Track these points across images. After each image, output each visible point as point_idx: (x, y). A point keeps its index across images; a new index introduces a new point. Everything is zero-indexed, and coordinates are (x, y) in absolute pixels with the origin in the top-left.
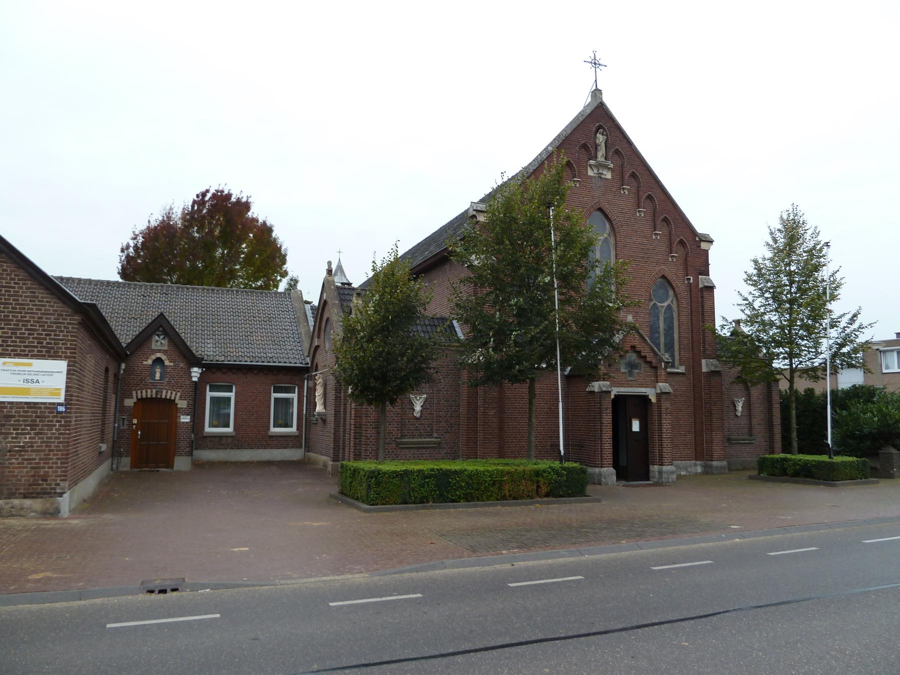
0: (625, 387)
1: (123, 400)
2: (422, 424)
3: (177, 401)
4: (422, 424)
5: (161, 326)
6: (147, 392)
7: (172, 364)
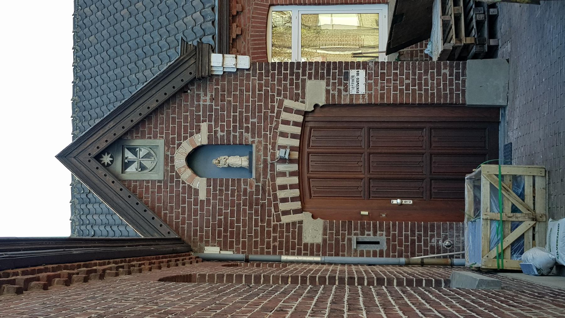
1: (306, 245)
3: (308, 107)
5: (98, 157)
6: (283, 187)
7: (204, 126)
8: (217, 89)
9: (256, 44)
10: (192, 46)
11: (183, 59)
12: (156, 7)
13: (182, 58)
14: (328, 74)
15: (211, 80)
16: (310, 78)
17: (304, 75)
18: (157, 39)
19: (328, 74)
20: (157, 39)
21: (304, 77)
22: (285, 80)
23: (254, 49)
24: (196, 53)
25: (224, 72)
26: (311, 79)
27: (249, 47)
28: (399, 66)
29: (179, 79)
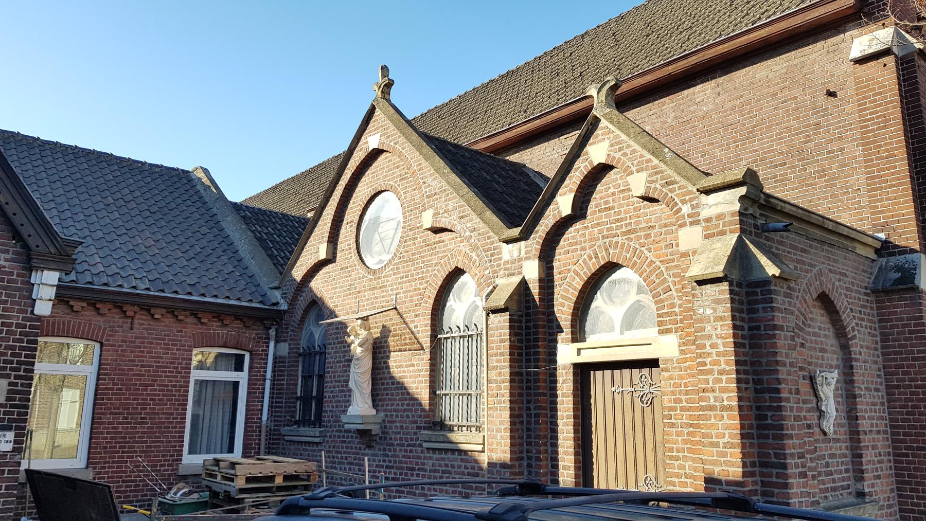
8: (12, 274)
9: (59, 324)
10: (73, 252)
11: (56, 239)
12: (113, 229)
13: (59, 239)
14: (12, 406)
15: (24, 269)
16: (10, 384)
17: (16, 377)
18: (78, 226)
19: (12, 406)
20: (78, 226)
21: (12, 377)
22: (12, 355)
23: (54, 323)
24: (62, 255)
25: (33, 285)
26: (9, 386)
27: (56, 317)
28: (10, 492)
29: (32, 232)
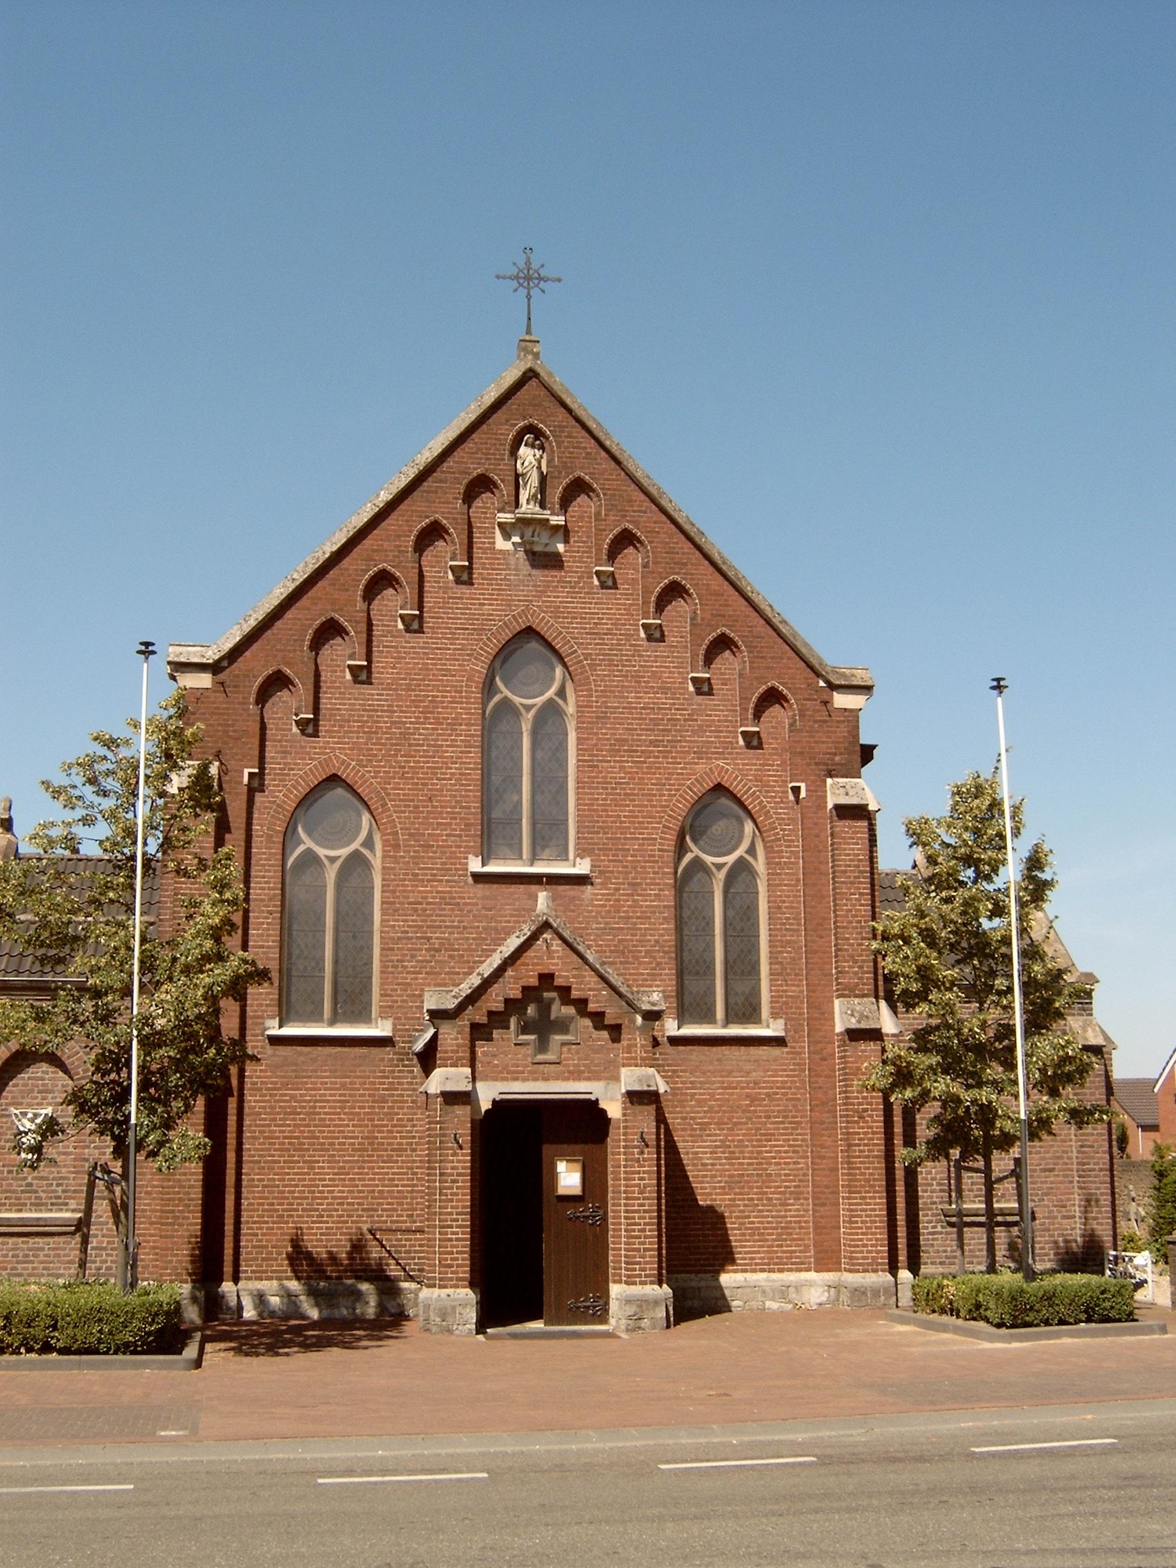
0: (525, 1080)
2: (42, 1178)
4: (42, 1178)
